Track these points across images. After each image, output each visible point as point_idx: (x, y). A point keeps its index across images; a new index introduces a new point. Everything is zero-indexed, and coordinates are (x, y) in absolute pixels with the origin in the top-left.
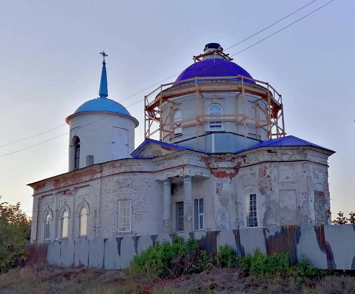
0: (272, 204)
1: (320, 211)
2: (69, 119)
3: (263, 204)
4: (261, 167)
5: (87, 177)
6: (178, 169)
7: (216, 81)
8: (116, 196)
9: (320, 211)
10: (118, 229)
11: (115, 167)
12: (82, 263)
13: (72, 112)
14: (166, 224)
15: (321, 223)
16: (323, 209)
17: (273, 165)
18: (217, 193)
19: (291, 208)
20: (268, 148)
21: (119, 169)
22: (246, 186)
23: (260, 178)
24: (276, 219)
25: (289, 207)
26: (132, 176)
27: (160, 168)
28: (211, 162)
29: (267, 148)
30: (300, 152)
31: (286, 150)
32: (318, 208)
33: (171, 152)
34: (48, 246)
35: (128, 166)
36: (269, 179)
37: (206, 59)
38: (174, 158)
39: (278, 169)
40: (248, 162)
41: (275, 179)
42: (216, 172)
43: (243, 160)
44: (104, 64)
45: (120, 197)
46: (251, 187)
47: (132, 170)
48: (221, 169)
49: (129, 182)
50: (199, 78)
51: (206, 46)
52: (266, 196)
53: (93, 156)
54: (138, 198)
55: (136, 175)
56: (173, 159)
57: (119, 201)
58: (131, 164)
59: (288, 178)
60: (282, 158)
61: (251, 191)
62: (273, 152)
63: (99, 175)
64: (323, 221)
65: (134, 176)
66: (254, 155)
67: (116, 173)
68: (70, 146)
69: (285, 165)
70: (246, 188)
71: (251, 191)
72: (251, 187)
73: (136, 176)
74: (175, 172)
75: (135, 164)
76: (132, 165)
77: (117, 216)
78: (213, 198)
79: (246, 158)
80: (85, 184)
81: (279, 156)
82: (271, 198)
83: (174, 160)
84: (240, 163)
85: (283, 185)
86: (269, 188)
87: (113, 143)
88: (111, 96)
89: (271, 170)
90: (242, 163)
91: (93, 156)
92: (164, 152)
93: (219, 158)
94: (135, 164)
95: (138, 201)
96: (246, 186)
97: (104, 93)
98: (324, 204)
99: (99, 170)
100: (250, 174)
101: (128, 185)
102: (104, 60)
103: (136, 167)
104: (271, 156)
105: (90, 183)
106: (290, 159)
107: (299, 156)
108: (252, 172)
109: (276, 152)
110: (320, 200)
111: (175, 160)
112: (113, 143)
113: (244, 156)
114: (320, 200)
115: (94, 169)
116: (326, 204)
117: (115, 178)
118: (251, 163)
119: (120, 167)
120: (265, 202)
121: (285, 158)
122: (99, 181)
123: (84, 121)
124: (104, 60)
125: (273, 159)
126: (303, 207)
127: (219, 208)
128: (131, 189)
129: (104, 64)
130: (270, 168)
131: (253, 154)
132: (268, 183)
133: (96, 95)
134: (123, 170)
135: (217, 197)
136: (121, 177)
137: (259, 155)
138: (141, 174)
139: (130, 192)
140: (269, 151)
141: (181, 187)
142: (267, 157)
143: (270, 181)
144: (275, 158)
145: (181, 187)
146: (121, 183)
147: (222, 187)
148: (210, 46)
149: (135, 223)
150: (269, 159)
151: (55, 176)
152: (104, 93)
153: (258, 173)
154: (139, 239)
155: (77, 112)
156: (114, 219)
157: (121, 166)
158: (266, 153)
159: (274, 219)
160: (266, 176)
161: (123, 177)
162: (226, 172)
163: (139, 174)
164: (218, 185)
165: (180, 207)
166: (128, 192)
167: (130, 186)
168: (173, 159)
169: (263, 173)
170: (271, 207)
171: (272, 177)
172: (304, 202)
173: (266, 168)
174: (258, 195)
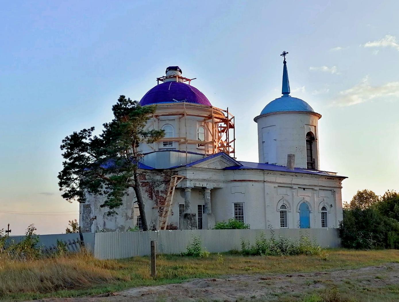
1: (86, 220)
2: (256, 120)
9: (86, 220)
12: (303, 255)
15: (86, 229)
16: (88, 218)
32: (85, 218)
44: (285, 62)
51: (167, 69)
64: (88, 228)
68: (307, 140)
88: (293, 93)
97: (286, 90)
98: (90, 214)
110: (87, 211)
114: (87, 211)
116: (91, 214)
123: (271, 120)
124: (285, 59)
129: (285, 62)
133: (279, 94)
148: (170, 69)
152: (286, 90)
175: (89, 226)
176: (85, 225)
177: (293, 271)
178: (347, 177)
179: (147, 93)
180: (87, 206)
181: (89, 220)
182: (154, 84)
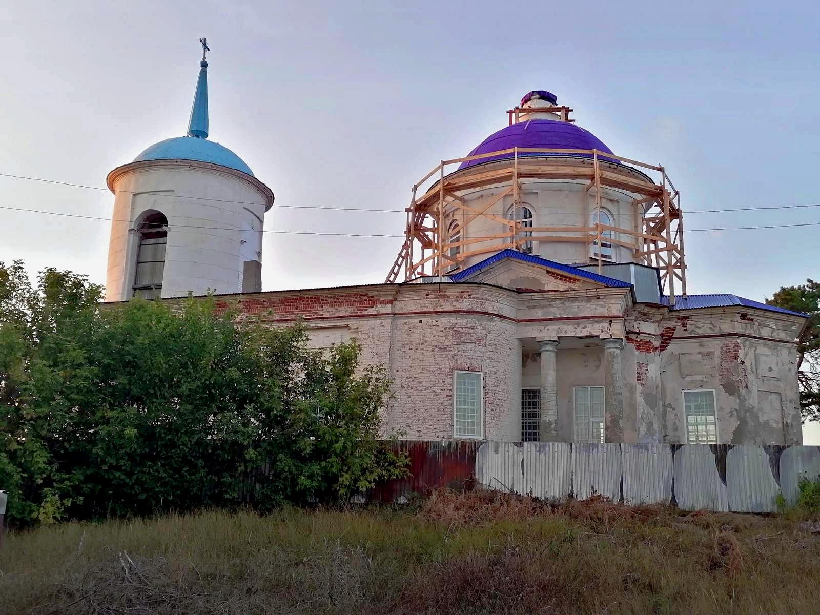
0: (748, 414)
3: (731, 412)
4: (726, 342)
5: (339, 309)
6: (596, 322)
7: (615, 167)
8: (447, 358)
10: (452, 430)
11: (445, 298)
13: (129, 158)
14: (553, 432)
17: (747, 343)
18: (638, 380)
19: (775, 425)
20: (745, 310)
21: (454, 304)
22: (687, 375)
23: (724, 364)
24: (756, 442)
25: (771, 422)
26: (485, 322)
27: (539, 314)
28: (628, 318)
29: (743, 310)
30: (787, 326)
31: (769, 320)
33: (575, 286)
34: (476, 450)
35: (478, 298)
36: (743, 367)
37: (539, 118)
38: (586, 299)
39: (755, 351)
40: (693, 331)
41: (752, 368)
42: (636, 339)
43: (680, 324)
44: (204, 65)
45: (459, 363)
46: (700, 378)
47: (484, 310)
48: (648, 336)
49: (480, 332)
50: (522, 150)
52: (740, 399)
53: (245, 262)
54: (495, 370)
55: (492, 321)
56: (582, 301)
57: (456, 372)
58: (485, 297)
59: (770, 369)
60: (760, 333)
61: (701, 386)
62: (749, 319)
63: (387, 309)
65: (489, 323)
66: (710, 319)
67: (446, 309)
69: (764, 346)
70: (688, 379)
71: (701, 386)
72: (700, 378)
73: (492, 324)
74: (585, 327)
75: (491, 299)
76: (486, 300)
77: (450, 402)
78: (632, 390)
79: (689, 323)
80: (334, 324)
81: (755, 327)
82: (747, 402)
83: (584, 303)
84: (674, 330)
85: (763, 382)
86: (744, 385)
87: (243, 242)
89: (746, 353)
90: (677, 330)
91: (245, 262)
92: (551, 283)
93: (645, 314)
94: (491, 299)
95: (496, 375)
96: (687, 375)
97: (199, 129)
99: (391, 298)
100: (699, 353)
101: (479, 341)
102: (204, 58)
103: (493, 303)
104: (744, 325)
105: (353, 323)
106: (771, 337)
107: (784, 333)
108: (704, 350)
109: (752, 320)
111: (585, 304)
112: (243, 242)
113: (687, 318)
115: (370, 294)
117: (444, 320)
118: (700, 332)
119: (457, 297)
120: (736, 410)
121: (765, 333)
122: (387, 322)
125: (747, 332)
126: (792, 425)
127: (642, 410)
128: (483, 349)
129: (204, 65)
130: (744, 347)
131: (710, 316)
132: (743, 375)
133: (181, 129)
134: (465, 305)
135: (639, 388)
136: (461, 322)
137: (721, 319)
138: (501, 321)
139: (480, 354)
140: (743, 316)
141: (535, 360)
142: (739, 326)
143: (744, 370)
144: (749, 331)
145: (535, 360)
146: (462, 333)
147: (647, 370)
149: (491, 421)
150: (741, 330)
151: (272, 291)
152: (199, 129)
153: (719, 353)
154: (785, 452)
155: (152, 157)
156: (441, 408)
157: (462, 297)
158: (737, 318)
159: (753, 442)
160: (739, 361)
161: (465, 321)
162: (653, 342)
163: (497, 320)
164: (640, 365)
165: (524, 401)
166: (478, 354)
167: (483, 343)
168: (582, 301)
169: (733, 355)
170: (748, 419)
171: (748, 364)
172: (794, 416)
173: (737, 345)
174: (718, 394)
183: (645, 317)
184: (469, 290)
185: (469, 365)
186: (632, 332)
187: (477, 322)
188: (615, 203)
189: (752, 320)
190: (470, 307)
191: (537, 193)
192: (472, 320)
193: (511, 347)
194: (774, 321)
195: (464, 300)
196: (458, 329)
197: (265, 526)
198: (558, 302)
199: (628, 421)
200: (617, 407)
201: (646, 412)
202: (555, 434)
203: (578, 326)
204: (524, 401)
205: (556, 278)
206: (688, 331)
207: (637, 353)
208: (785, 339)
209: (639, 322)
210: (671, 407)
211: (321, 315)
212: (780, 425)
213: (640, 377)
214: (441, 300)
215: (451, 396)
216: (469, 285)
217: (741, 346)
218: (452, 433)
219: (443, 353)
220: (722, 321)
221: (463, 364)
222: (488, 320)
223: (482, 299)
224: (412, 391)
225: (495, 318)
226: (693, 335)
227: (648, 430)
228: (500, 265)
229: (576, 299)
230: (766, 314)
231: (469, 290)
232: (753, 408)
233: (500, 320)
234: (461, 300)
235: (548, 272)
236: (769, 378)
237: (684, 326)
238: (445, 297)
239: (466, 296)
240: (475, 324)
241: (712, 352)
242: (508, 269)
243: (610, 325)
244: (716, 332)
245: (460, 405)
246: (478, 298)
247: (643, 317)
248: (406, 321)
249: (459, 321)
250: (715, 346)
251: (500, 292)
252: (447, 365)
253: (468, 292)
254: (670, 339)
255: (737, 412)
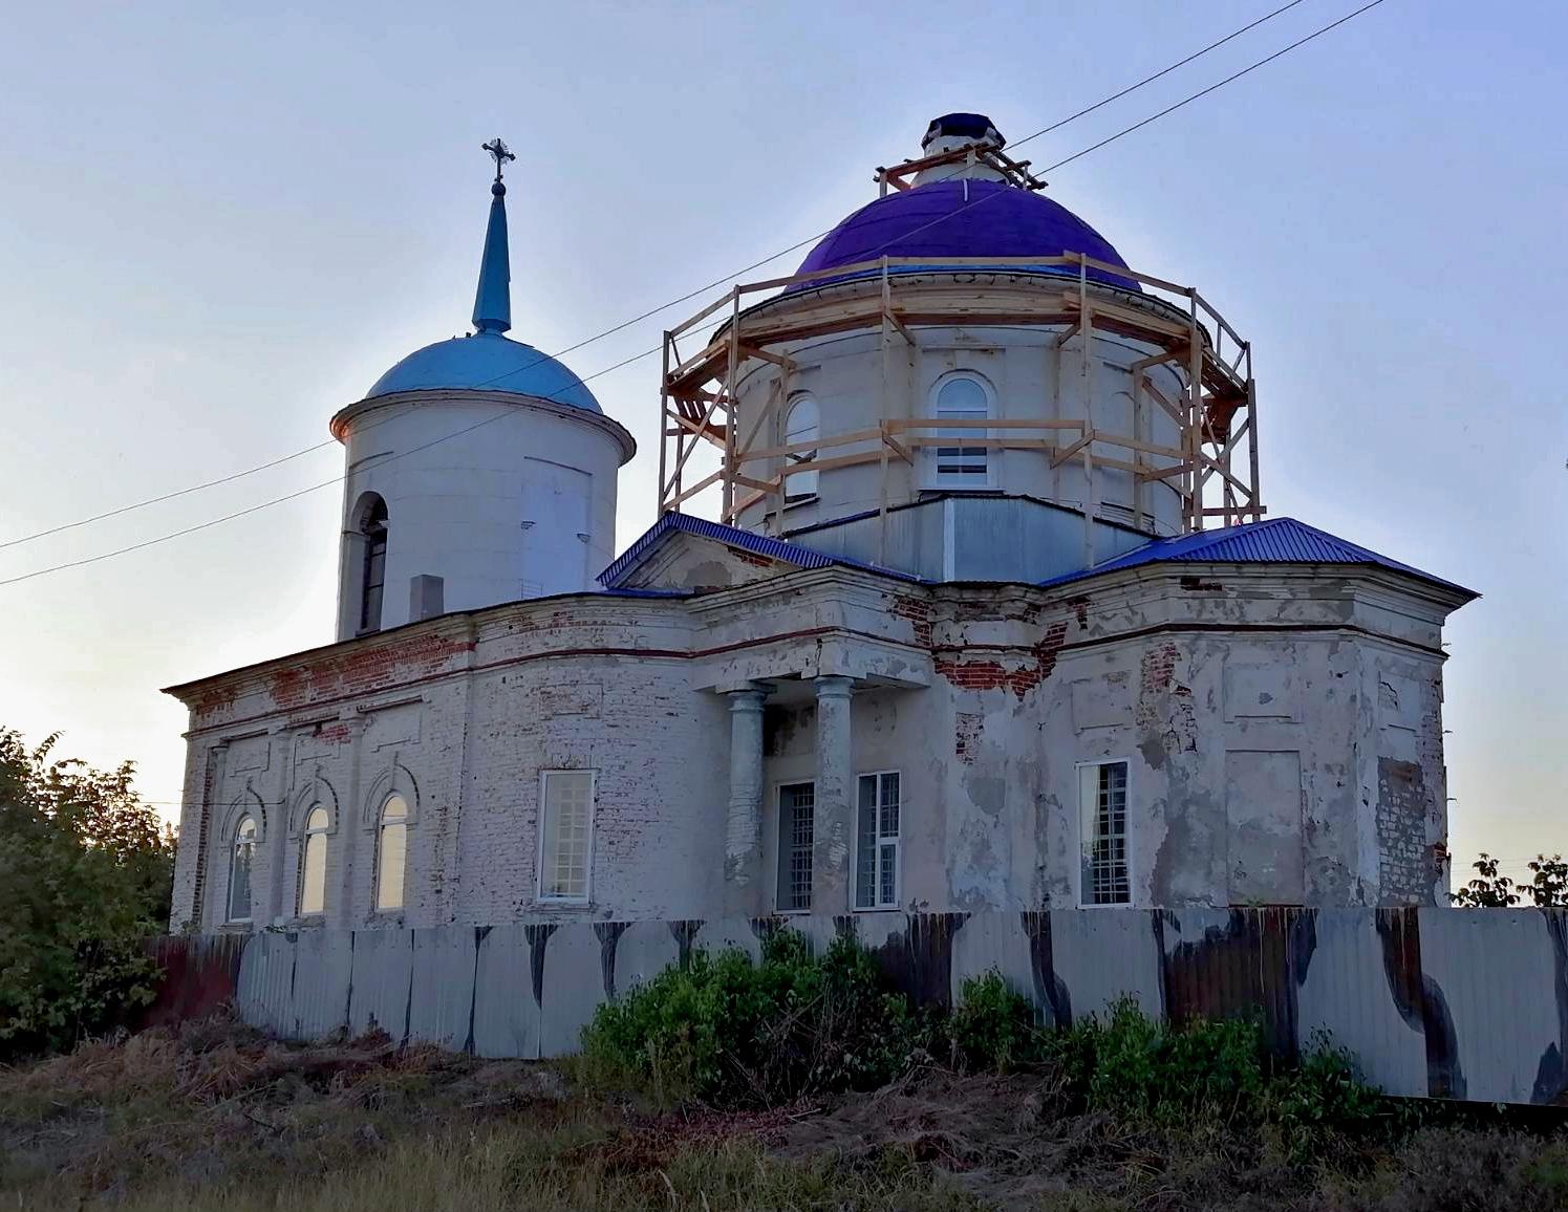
1: (1401, 845)
2: (345, 421)
3: (1155, 806)
4: (1151, 647)
7: (971, 277)
14: (738, 878)
16: (1416, 840)
17: (1203, 643)
18: (958, 752)
19: (1278, 829)
21: (546, 640)
27: (722, 637)
30: (1324, 588)
31: (1264, 581)
35: (585, 623)
36: (1185, 700)
39: (1225, 659)
40: (1098, 627)
42: (957, 663)
44: (499, 190)
45: (549, 755)
47: (600, 645)
49: (586, 693)
50: (899, 261)
51: (934, 125)
52: (1170, 776)
55: (616, 663)
62: (1208, 587)
63: (462, 660)
64: (1411, 890)
65: (609, 669)
66: (1125, 598)
71: (1107, 752)
72: (1104, 733)
75: (614, 620)
76: (604, 623)
78: (940, 773)
81: (1230, 603)
84: (1064, 630)
85: (1244, 730)
86: (1186, 742)
88: (526, 327)
90: (1069, 629)
93: (973, 605)
95: (623, 773)
98: (1422, 819)
99: (466, 639)
101: (585, 708)
107: (1318, 605)
108: (1114, 669)
109: (1219, 588)
113: (1081, 600)
116: (1427, 819)
117: (531, 673)
118: (1110, 628)
119: (550, 626)
120: (1164, 801)
121: (1257, 613)
123: (408, 428)
125: (1205, 618)
126: (1327, 826)
129: (499, 190)
130: (1192, 653)
131: (1120, 591)
132: (1183, 718)
133: (457, 321)
134: (563, 640)
135: (957, 768)
136: (554, 673)
137: (1143, 595)
140: (1190, 583)
142: (1176, 605)
147: (981, 727)
148: (951, 125)
150: (1190, 616)
151: (1306, 523)
157: (557, 626)
158: (1176, 589)
161: (562, 671)
164: (965, 718)
167: (592, 711)
170: (1190, 821)
172: (1334, 803)
173: (1171, 652)
175: (1421, 881)
176: (1391, 872)
177: (986, 1181)
178: (164, 691)
179: (1084, 222)
180: (1409, 775)
181: (1421, 850)
182: (870, 193)
183: (979, 611)
184: (567, 609)
185: (565, 759)
186: (951, 649)
187: (583, 671)
188: (997, 355)
189: (1219, 588)
190: (571, 643)
191: (819, 367)
192: (575, 668)
193: (671, 711)
194: (1281, 581)
195: (563, 629)
196: (549, 690)
197: (813, 1010)
198: (745, 609)
199: (933, 842)
200: (824, 821)
201: (973, 820)
202: (742, 883)
203: (775, 656)
204: (808, 806)
205: (744, 560)
206: (1090, 629)
207: (957, 691)
208: (1322, 621)
209: (965, 623)
210: (1056, 803)
211: (393, 681)
212: (1295, 829)
213: (963, 745)
214: (529, 633)
215: (534, 822)
216: (563, 600)
217: (1183, 652)
218: (534, 893)
219: (528, 738)
220: (1145, 599)
221: (556, 758)
222: (607, 664)
223: (595, 623)
224: (490, 815)
225: (622, 658)
226: (1097, 637)
227: (977, 858)
228: (669, 544)
229: (766, 600)
230: (1245, 570)
231: (567, 609)
232: (1208, 793)
233: (637, 661)
234: (557, 629)
235: (731, 549)
236: (1260, 721)
237: (1082, 618)
238: (531, 627)
239: (562, 621)
240: (581, 674)
241: (1124, 673)
242: (683, 549)
243: (820, 647)
244: (1137, 625)
245: (801, 804)
246: (585, 623)
247: (973, 611)
248: (488, 680)
249: (552, 673)
250: (1131, 656)
251: (627, 604)
252: (532, 761)
253: (565, 613)
254: (1054, 652)
255: (1165, 806)
